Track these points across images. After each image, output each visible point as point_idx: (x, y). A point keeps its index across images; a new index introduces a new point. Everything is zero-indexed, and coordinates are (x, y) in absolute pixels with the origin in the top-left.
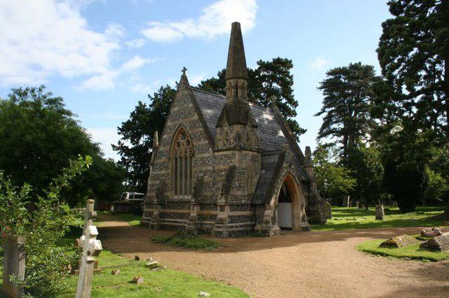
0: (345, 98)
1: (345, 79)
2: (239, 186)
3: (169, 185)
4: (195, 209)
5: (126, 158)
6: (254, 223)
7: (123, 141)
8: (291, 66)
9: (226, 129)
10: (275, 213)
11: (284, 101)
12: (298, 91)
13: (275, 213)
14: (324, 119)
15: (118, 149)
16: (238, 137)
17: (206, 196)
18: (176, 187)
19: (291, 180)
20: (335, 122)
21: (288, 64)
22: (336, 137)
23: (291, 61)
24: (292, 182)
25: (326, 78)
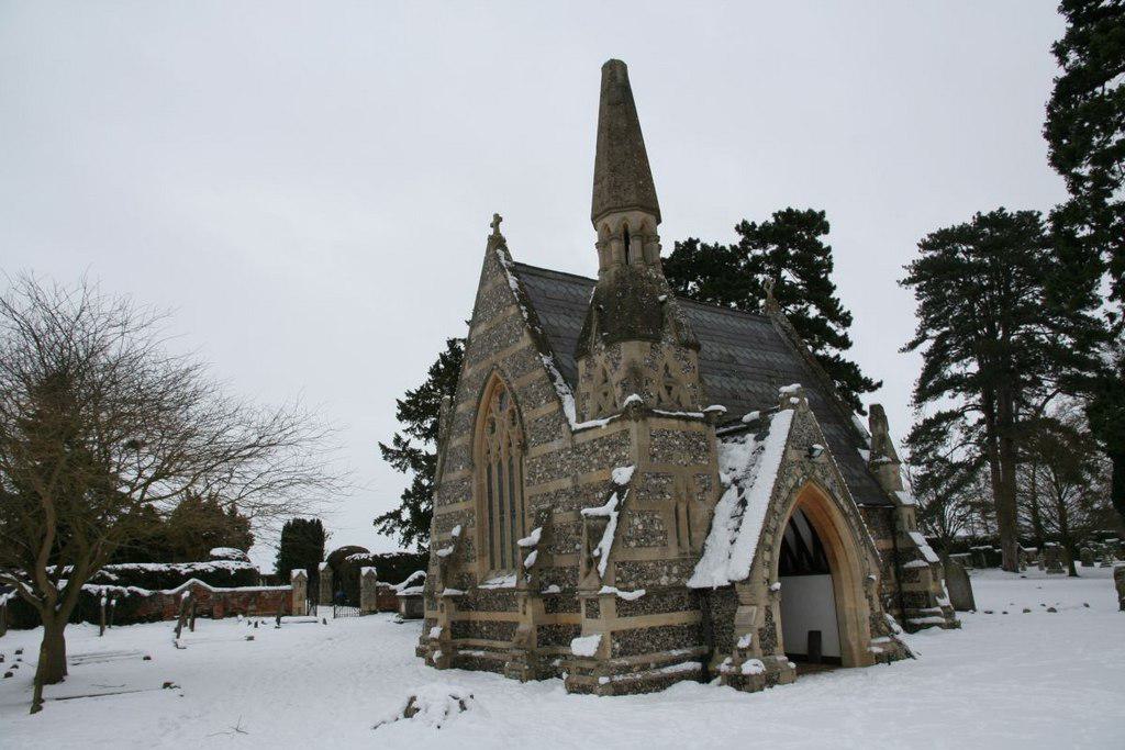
0: (974, 298)
1: (967, 253)
2: (645, 532)
3: (476, 543)
4: (529, 609)
5: (425, 482)
6: (705, 649)
7: (405, 438)
8: (825, 228)
9: (600, 359)
10: (769, 614)
11: (813, 312)
12: (846, 285)
13: (769, 614)
14: (927, 355)
15: (398, 455)
16: (635, 379)
17: (562, 569)
18: (492, 545)
19: (817, 500)
20: (957, 359)
21: (815, 222)
22: (961, 396)
23: (823, 213)
24: (825, 510)
25: (920, 256)
